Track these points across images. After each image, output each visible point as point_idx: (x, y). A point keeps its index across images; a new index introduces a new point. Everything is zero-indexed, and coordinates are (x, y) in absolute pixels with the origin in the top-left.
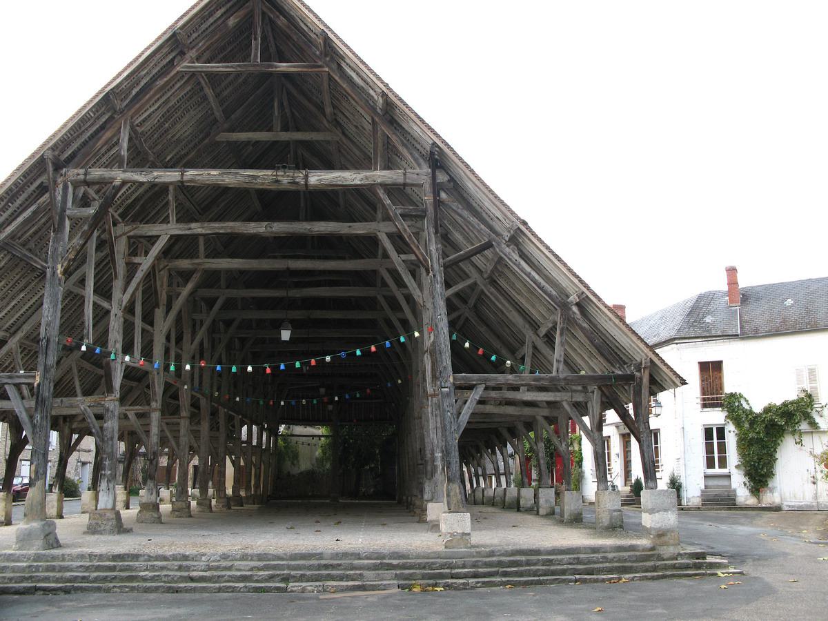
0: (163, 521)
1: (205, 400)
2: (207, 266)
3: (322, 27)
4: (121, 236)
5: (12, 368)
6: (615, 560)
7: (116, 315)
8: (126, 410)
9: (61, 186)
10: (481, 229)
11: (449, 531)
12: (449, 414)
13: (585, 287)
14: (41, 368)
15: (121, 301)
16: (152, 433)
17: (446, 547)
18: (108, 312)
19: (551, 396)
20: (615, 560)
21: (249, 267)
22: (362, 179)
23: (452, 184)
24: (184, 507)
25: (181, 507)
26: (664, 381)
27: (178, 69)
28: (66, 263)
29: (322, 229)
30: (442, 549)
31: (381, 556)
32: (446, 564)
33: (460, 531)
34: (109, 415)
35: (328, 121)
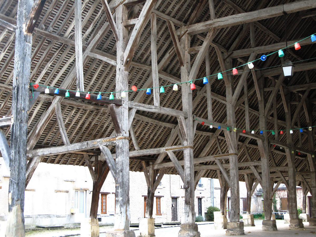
1: (261, 140)
2: (217, 25)
4: (119, 5)
5: (178, 140)
7: (120, 69)
8: (166, 150)
14: (14, 111)
16: (186, 167)
21: (251, 18)
24: (236, 226)
25: (233, 227)
28: (29, 21)
34: (119, 151)
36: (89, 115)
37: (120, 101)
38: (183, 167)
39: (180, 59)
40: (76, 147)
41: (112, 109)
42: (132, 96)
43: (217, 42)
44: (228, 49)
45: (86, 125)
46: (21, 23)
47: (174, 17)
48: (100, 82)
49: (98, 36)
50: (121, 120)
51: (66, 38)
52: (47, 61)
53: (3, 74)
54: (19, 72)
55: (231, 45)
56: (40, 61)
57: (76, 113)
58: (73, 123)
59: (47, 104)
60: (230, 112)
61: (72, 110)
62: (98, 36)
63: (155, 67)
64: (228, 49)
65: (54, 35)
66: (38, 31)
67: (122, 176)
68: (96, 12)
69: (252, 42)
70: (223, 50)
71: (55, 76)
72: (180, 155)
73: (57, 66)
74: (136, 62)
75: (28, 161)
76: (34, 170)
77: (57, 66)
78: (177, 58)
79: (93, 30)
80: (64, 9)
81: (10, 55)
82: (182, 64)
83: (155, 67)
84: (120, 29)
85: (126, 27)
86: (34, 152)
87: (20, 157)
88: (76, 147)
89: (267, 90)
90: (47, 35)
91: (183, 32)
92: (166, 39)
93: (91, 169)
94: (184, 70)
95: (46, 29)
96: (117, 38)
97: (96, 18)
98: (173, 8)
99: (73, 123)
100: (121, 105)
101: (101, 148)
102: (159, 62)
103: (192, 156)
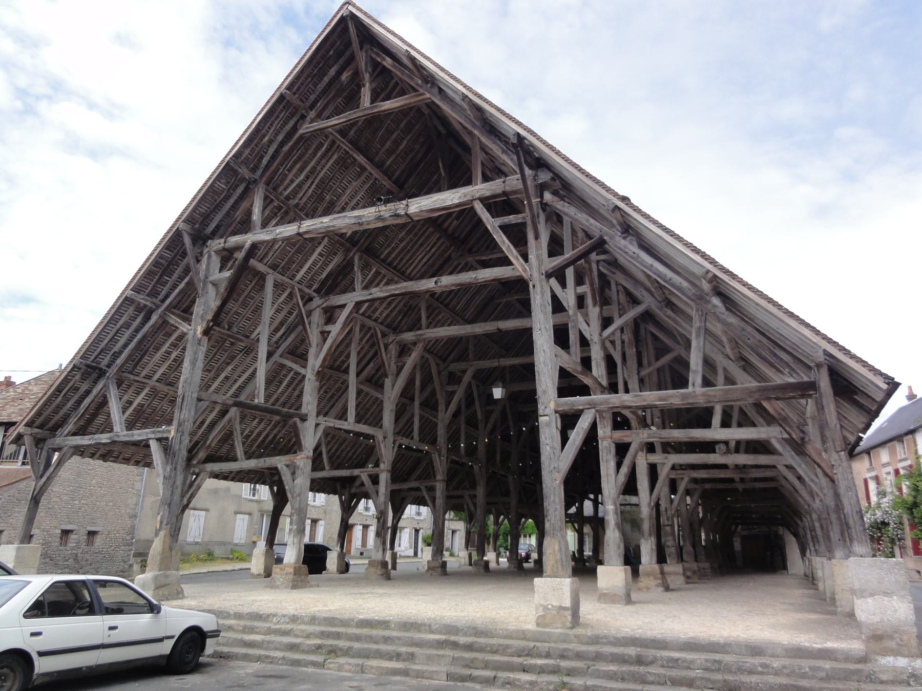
0: (671, 587)
2: (427, 335)
3: (405, 47)
6: (785, 671)
9: (206, 256)
10: (591, 225)
11: (542, 603)
12: (548, 448)
13: (711, 263)
14: (175, 422)
15: (314, 366)
17: (538, 625)
18: (304, 376)
19: (752, 433)
20: (785, 671)
22: (460, 198)
23: (558, 181)
26: (866, 386)
27: (301, 131)
29: (487, 275)
30: (531, 626)
31: (451, 629)
32: (524, 649)
33: (556, 604)
35: (490, 170)
36: (275, 426)
37: (306, 415)
38: (377, 492)
39: (385, 370)
40: (252, 464)
41: (295, 423)
42: (322, 411)
43: (432, 353)
44: (444, 360)
45: (270, 438)
46: (196, 325)
47: (382, 323)
48: (290, 390)
49: (290, 340)
50: (304, 437)
51: (253, 340)
52: (228, 364)
53: (173, 375)
54: (187, 379)
55: (449, 355)
56: (219, 363)
57: (259, 423)
58: (255, 434)
59: (224, 413)
60: (441, 431)
61: (254, 419)
62: (290, 340)
63: (352, 378)
64: (444, 360)
65: (238, 336)
66: (219, 332)
67: (300, 501)
68: (290, 313)
69: (471, 355)
70: (439, 362)
71: (236, 381)
72: (375, 480)
73: (240, 369)
74: (336, 370)
75: (194, 477)
76: (199, 487)
77: (240, 369)
78: (382, 370)
79: (285, 333)
80: (253, 308)
81: (180, 359)
82: (386, 376)
83: (352, 378)
84: (314, 336)
85: (322, 333)
86: (201, 466)
87: (176, 474)
88: (252, 464)
89: (488, 408)
90: (229, 336)
91: (390, 340)
92: (372, 346)
93: (271, 489)
94: (388, 382)
95: (228, 330)
96: (310, 344)
97: (290, 320)
98: (381, 314)
99: (255, 434)
100: (306, 420)
101: (279, 467)
102: (358, 375)
103: (389, 481)
